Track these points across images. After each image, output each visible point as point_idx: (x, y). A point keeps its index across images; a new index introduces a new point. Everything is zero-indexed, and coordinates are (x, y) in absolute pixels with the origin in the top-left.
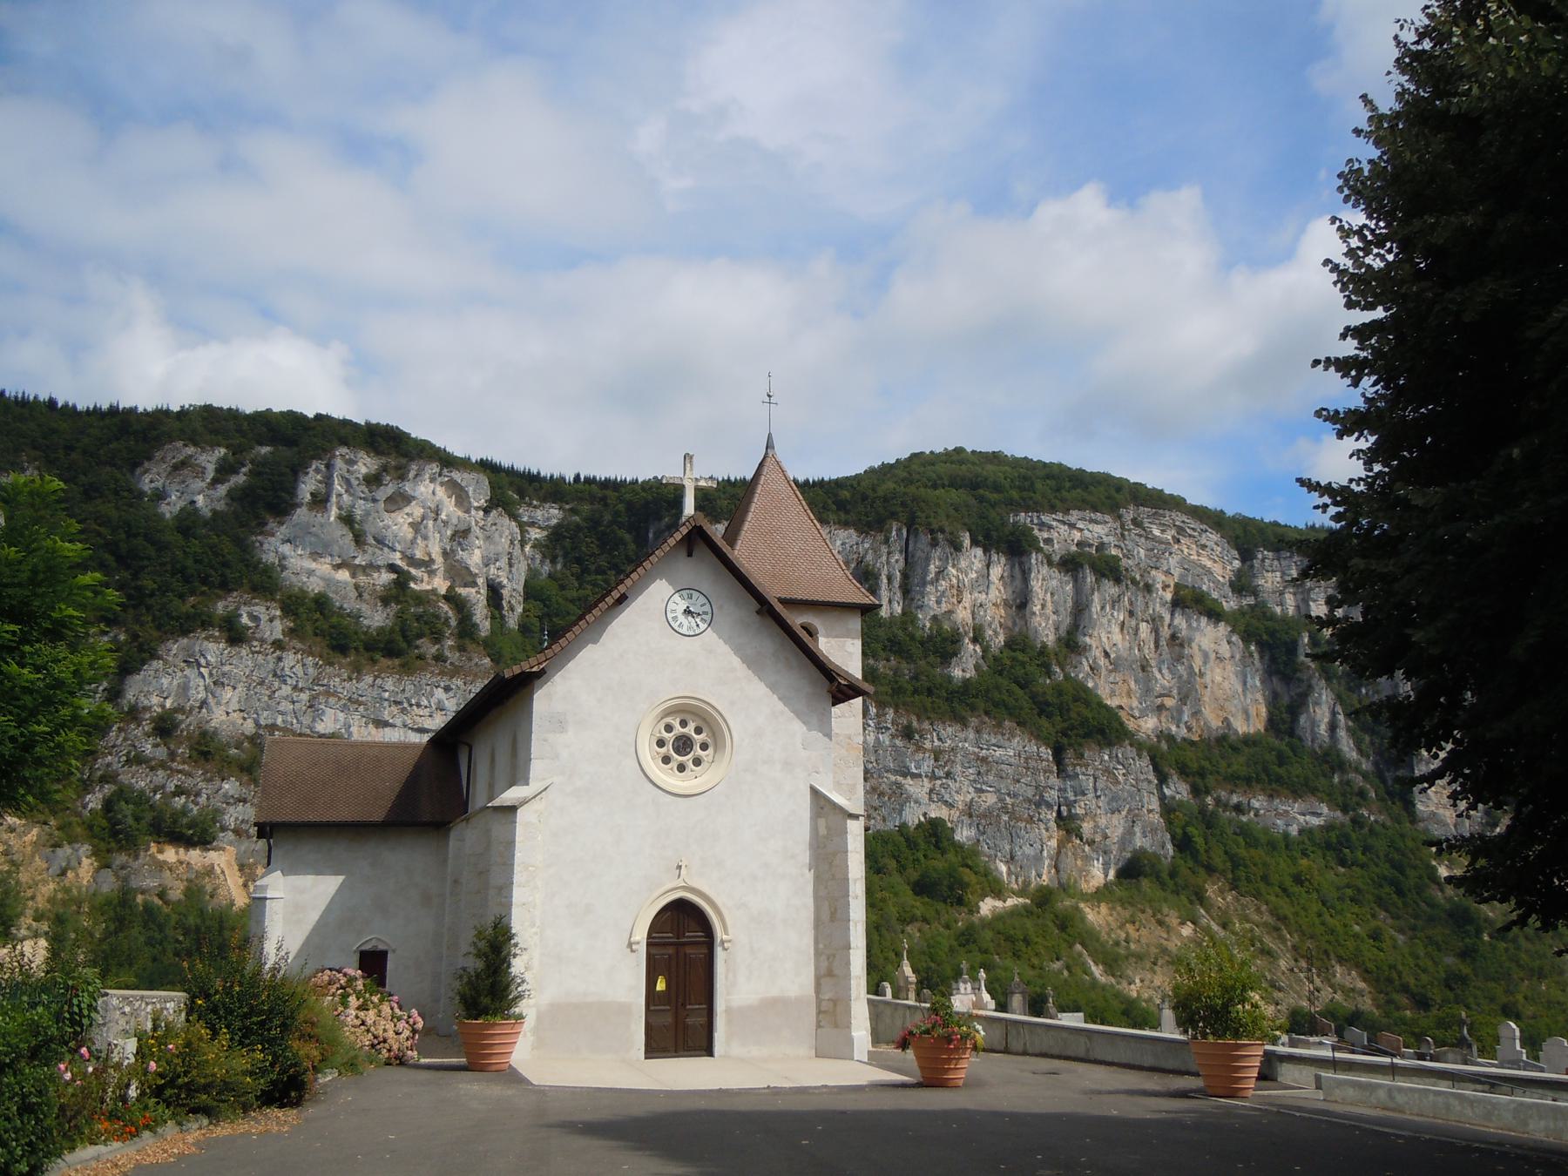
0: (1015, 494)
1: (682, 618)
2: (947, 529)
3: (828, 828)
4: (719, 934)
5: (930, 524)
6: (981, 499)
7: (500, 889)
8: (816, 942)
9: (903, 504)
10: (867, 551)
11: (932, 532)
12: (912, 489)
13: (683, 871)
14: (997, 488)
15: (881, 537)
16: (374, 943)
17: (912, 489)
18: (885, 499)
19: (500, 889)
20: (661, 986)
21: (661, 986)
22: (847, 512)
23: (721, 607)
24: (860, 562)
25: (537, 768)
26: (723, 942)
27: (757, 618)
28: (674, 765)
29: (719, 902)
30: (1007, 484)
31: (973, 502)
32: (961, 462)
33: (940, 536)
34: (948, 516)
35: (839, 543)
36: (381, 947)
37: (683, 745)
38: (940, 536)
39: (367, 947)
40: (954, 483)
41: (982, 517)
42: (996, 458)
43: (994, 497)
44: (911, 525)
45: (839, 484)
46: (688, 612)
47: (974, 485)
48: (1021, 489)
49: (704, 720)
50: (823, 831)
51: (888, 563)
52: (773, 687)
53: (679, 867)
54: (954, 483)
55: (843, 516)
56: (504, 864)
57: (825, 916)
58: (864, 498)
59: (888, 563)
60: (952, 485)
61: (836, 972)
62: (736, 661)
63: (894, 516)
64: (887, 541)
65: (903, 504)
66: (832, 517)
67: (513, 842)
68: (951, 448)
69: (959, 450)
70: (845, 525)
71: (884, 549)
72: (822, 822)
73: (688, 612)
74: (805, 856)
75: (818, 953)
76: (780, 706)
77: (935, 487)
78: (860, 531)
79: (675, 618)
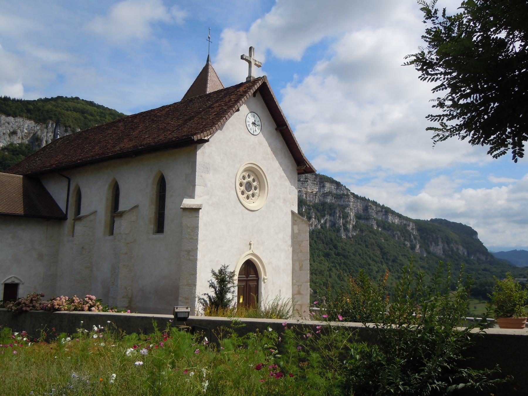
0: (98, 118)
1: (251, 125)
2: (72, 126)
3: (299, 230)
4: (263, 276)
5: (65, 124)
6: (85, 118)
7: (189, 252)
8: (293, 280)
9: (55, 115)
10: (38, 130)
11: (66, 127)
12: (59, 109)
13: (252, 246)
14: (92, 115)
15: (44, 126)
16: (13, 279)
17: (59, 109)
18: (47, 111)
19: (189, 252)
20: (241, 301)
21: (241, 301)
22: (31, 114)
23: (264, 124)
24: (34, 134)
25: (198, 189)
26: (264, 279)
27: (275, 131)
28: (245, 195)
29: (264, 260)
30: (95, 113)
31: (82, 118)
32: (78, 103)
33: (69, 129)
34: (72, 122)
35: (26, 125)
36: (17, 281)
37: (249, 186)
38: (69, 129)
39: (9, 282)
40: (75, 110)
41: (85, 124)
42: (91, 104)
43: (90, 117)
44: (58, 123)
45: (29, 102)
46: (254, 124)
47: (83, 112)
48: (101, 116)
49: (256, 176)
50: (296, 231)
51: (47, 136)
52: (281, 164)
53: (250, 244)
54: (75, 110)
55: (29, 115)
56: (192, 239)
57: (297, 269)
58: (39, 110)
59: (47, 136)
60: (74, 111)
61: (302, 292)
62: (269, 150)
63: (51, 118)
64: (47, 127)
65: (55, 115)
66: (24, 115)
67: (197, 227)
68: (74, 97)
69: (77, 98)
70: (30, 119)
71: (45, 130)
72: (296, 227)
73: (254, 124)
74: (289, 242)
75: (293, 284)
76: (283, 174)
77: (67, 110)
78: (36, 122)
79: (249, 125)
